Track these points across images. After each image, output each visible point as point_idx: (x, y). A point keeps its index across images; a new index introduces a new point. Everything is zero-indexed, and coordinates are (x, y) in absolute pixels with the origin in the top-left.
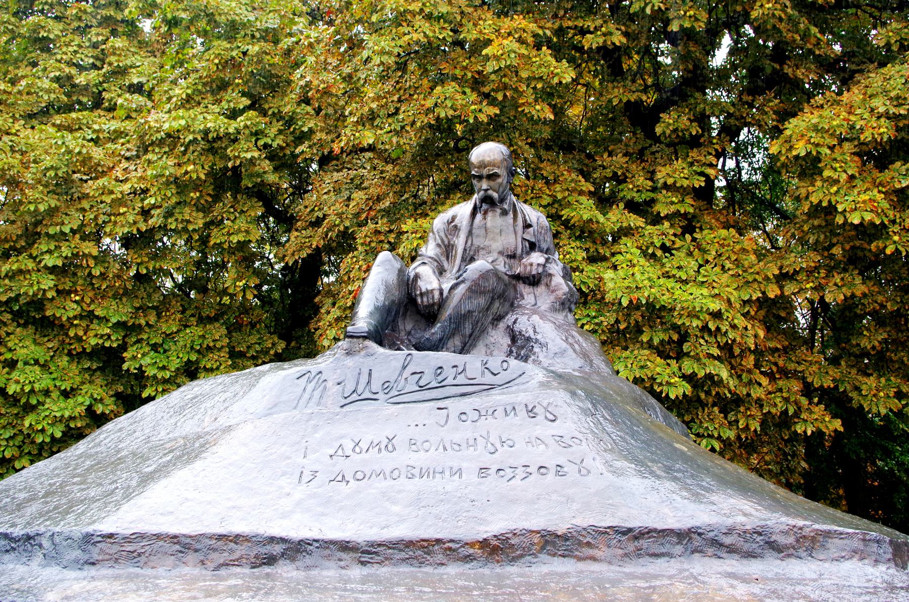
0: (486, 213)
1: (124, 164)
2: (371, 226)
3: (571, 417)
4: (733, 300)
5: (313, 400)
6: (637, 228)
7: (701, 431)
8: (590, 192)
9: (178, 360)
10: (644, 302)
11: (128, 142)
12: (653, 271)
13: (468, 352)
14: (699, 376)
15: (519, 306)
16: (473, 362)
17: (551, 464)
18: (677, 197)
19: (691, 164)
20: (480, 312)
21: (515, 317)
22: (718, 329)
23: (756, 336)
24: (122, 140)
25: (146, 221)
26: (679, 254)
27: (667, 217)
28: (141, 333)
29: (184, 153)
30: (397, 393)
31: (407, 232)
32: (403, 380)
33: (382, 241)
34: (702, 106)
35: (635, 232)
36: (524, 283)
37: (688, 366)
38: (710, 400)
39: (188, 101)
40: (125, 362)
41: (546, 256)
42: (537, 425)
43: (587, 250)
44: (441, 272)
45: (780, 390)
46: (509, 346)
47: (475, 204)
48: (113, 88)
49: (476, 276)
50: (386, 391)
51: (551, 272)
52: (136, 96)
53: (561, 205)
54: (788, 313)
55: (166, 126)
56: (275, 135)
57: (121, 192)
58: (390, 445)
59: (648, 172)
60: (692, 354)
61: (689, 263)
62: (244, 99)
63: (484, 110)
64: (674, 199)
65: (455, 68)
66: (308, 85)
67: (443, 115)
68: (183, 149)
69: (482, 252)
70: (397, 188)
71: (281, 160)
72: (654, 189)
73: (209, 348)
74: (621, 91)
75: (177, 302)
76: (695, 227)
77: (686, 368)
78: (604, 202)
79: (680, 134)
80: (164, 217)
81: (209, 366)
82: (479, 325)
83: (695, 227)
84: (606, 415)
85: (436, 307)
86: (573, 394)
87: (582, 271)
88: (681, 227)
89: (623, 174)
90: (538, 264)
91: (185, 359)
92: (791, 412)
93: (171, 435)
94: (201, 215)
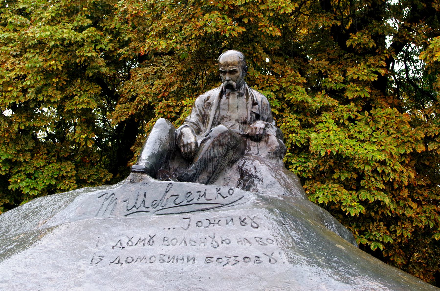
0: (228, 95)
1: (12, 60)
2: (165, 102)
3: (268, 226)
4: (393, 154)
5: (108, 211)
6: (333, 107)
7: (371, 237)
8: (304, 83)
9: (44, 184)
10: (335, 154)
11: (15, 46)
12: (342, 134)
13: (212, 183)
14: (370, 202)
15: (247, 154)
16: (211, 189)
17: (252, 255)
18: (359, 87)
19: (369, 66)
20: (219, 158)
21: (243, 161)
22: (383, 172)
23: (409, 177)
24: (11, 45)
25: (25, 96)
26: (360, 123)
27: (353, 100)
28: (20, 167)
29: (50, 53)
30: (161, 208)
31: (186, 106)
32: (165, 200)
33: (171, 112)
34: (376, 29)
35: (332, 109)
36: (252, 140)
37: (364, 195)
38: (378, 217)
39: (52, 21)
40: (10, 184)
41: (266, 123)
42: (246, 230)
43: (301, 120)
44: (198, 132)
45: (425, 212)
46: (239, 179)
47: (222, 89)
48: (7, 11)
49: (217, 135)
50: (154, 207)
51: (268, 133)
52: (20, 17)
53: (285, 91)
54: (431, 163)
55: (38, 35)
56: (108, 44)
57: (9, 78)
58: (151, 241)
59: (342, 71)
60: (366, 187)
61: (366, 129)
62: (88, 20)
63: (235, 29)
64: (357, 88)
65: (219, 2)
66: (125, 12)
67: (209, 31)
68: (48, 50)
69: (225, 120)
70: (181, 78)
71: (111, 59)
72: (345, 82)
73: (63, 177)
74: (324, 19)
75: (44, 147)
76: (372, 107)
77: (362, 196)
78: (314, 90)
79: (362, 46)
80: (36, 93)
81: (63, 188)
82: (219, 165)
83: (372, 107)
84: (292, 225)
85: (193, 154)
86: (271, 211)
87: (297, 133)
88: (362, 106)
89: (326, 72)
90: (260, 128)
91: (48, 184)
92: (431, 226)
93: (17, 232)
94: (59, 92)
